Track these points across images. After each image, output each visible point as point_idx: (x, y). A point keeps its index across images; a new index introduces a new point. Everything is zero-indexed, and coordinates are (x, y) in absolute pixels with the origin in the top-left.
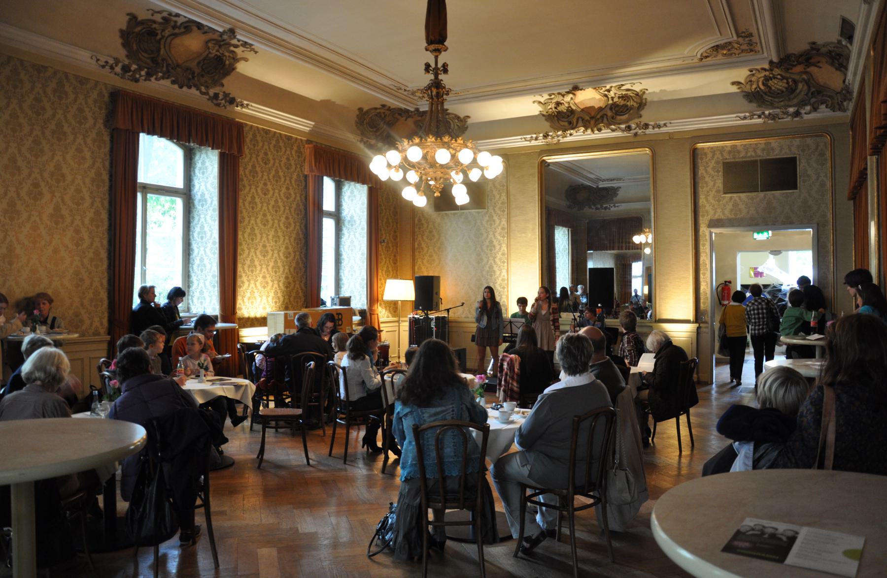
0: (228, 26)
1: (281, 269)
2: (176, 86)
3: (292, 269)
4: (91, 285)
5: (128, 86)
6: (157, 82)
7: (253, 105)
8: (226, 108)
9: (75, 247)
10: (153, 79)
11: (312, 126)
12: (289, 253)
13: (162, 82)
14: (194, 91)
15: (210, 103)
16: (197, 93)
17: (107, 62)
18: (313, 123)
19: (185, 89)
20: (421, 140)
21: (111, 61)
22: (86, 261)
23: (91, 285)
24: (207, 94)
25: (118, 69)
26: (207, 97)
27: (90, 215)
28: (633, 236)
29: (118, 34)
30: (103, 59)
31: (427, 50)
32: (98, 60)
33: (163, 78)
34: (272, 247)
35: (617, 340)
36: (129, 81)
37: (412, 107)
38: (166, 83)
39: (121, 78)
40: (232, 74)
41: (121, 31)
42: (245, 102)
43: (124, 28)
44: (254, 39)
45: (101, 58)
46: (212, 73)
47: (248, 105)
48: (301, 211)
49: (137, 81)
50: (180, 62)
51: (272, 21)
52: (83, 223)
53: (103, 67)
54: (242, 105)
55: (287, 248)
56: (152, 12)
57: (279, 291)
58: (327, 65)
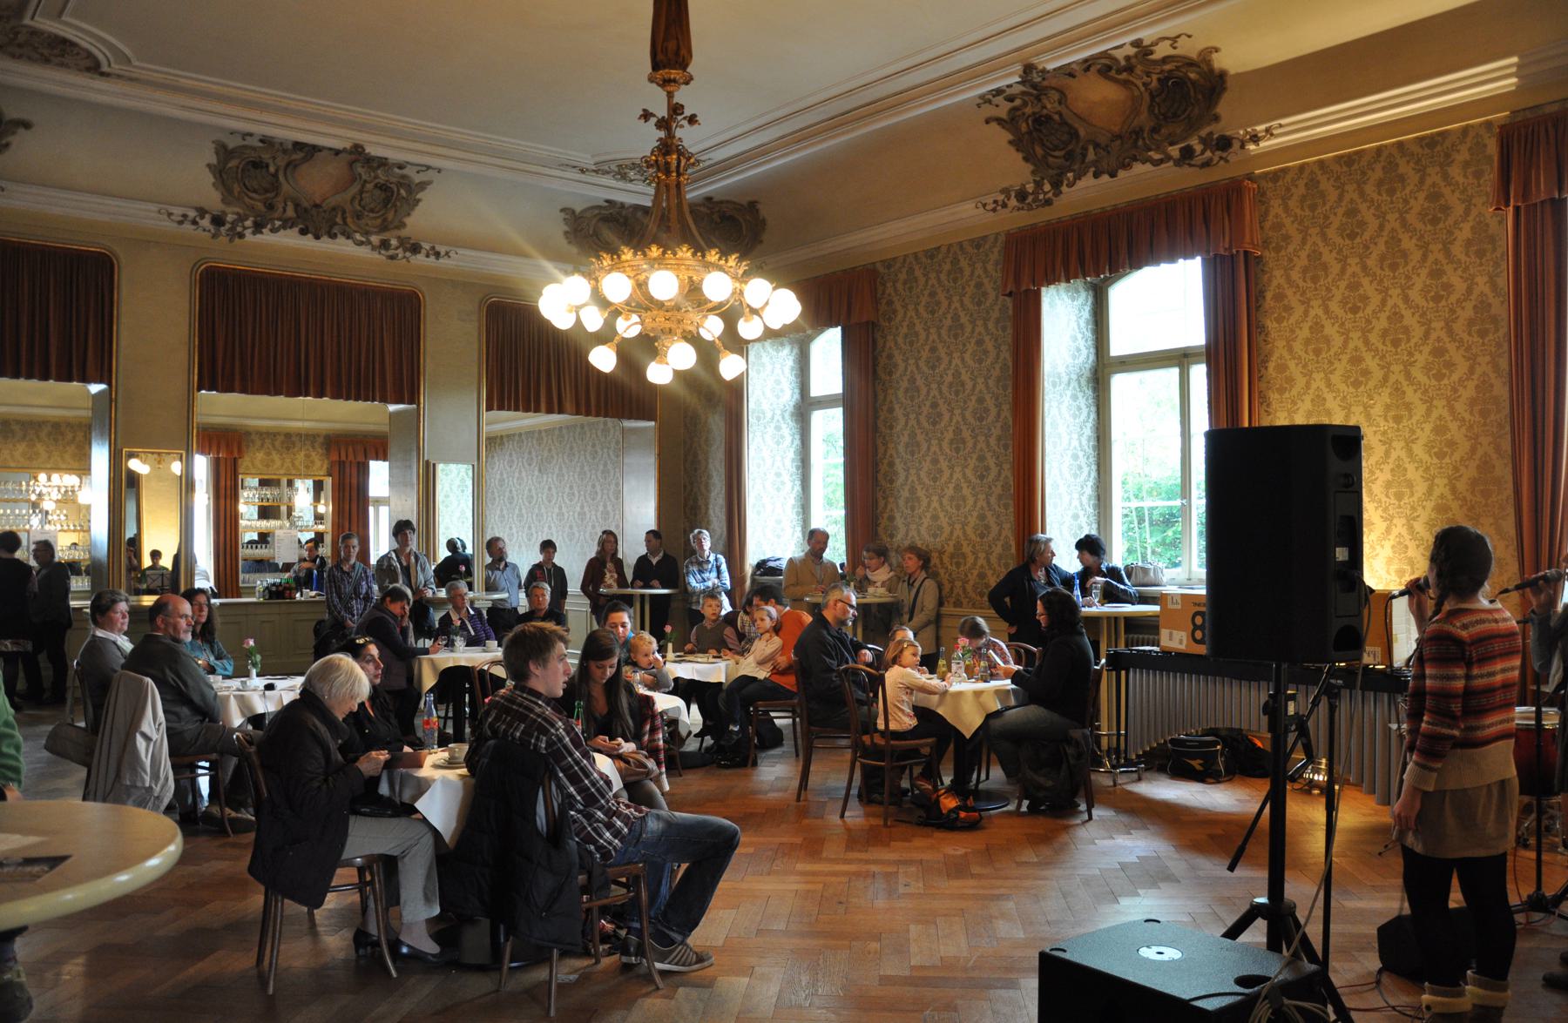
0: (1019, 68)
1: (1421, 488)
2: (1106, 178)
3: (1462, 486)
4: (1000, 534)
5: (1042, 216)
6: (1073, 188)
7: (1283, 121)
8: (1227, 161)
9: (978, 481)
10: (1064, 188)
11: (1514, 70)
12: (1452, 444)
13: (1081, 184)
14: (1139, 168)
15: (1186, 170)
16: (1148, 166)
17: (995, 202)
18: (1515, 60)
19: (1122, 174)
20: (664, 253)
21: (1001, 197)
22: (993, 500)
23: (1000, 534)
24: (1169, 158)
25: (1013, 202)
26: (1171, 163)
27: (996, 432)
28: (1051, 280)
29: (1012, 149)
30: (989, 200)
31: (651, 80)
32: (984, 205)
33: (1078, 177)
34: (1384, 433)
35: (1129, 923)
36: (1041, 209)
37: (1011, 74)
38: (1088, 181)
39: (1028, 210)
40: (1229, 84)
41: (1010, 142)
42: (1261, 128)
43: (1011, 137)
44: (764, 162)
45: (987, 201)
46: (1185, 110)
47: (1268, 130)
48: (1059, 378)
49: (1048, 202)
50: (1116, 129)
51: (997, 31)
52: (988, 445)
53: (994, 210)
54: (1255, 139)
55: (1439, 430)
56: (1169, 42)
57: (1412, 545)
58: (1096, 33)
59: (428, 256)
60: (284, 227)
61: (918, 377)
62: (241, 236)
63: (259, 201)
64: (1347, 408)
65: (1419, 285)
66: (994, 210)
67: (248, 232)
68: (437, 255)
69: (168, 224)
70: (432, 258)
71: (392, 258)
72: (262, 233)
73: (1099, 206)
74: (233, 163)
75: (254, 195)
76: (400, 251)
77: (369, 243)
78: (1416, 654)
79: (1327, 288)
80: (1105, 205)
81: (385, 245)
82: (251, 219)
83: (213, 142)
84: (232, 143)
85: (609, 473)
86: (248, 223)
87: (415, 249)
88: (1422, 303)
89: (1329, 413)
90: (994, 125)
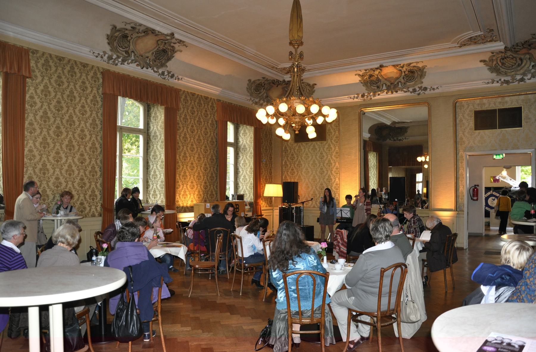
24: (409, 91)
32: (94, 53)
45: (95, 52)
59: (176, 79)
60: (132, 62)
61: (157, 171)
62: (117, 65)
63: (123, 51)
64: (291, 179)
65: (77, 158)
66: (97, 57)
67: (119, 64)
68: (179, 79)
69: (92, 57)
70: (177, 80)
71: (164, 78)
72: (124, 64)
73: (27, 46)
74: (116, 34)
75: (374, 85)
76: (420, 91)
77: (409, 91)
78: (350, 315)
79: (49, 152)
80: (18, 44)
81: (414, 91)
82: (121, 58)
83: (111, 25)
84: (119, 26)
85: (187, 196)
86: (120, 60)
87: (172, 76)
88: (53, 187)
89: (287, 180)
90: (357, 76)
